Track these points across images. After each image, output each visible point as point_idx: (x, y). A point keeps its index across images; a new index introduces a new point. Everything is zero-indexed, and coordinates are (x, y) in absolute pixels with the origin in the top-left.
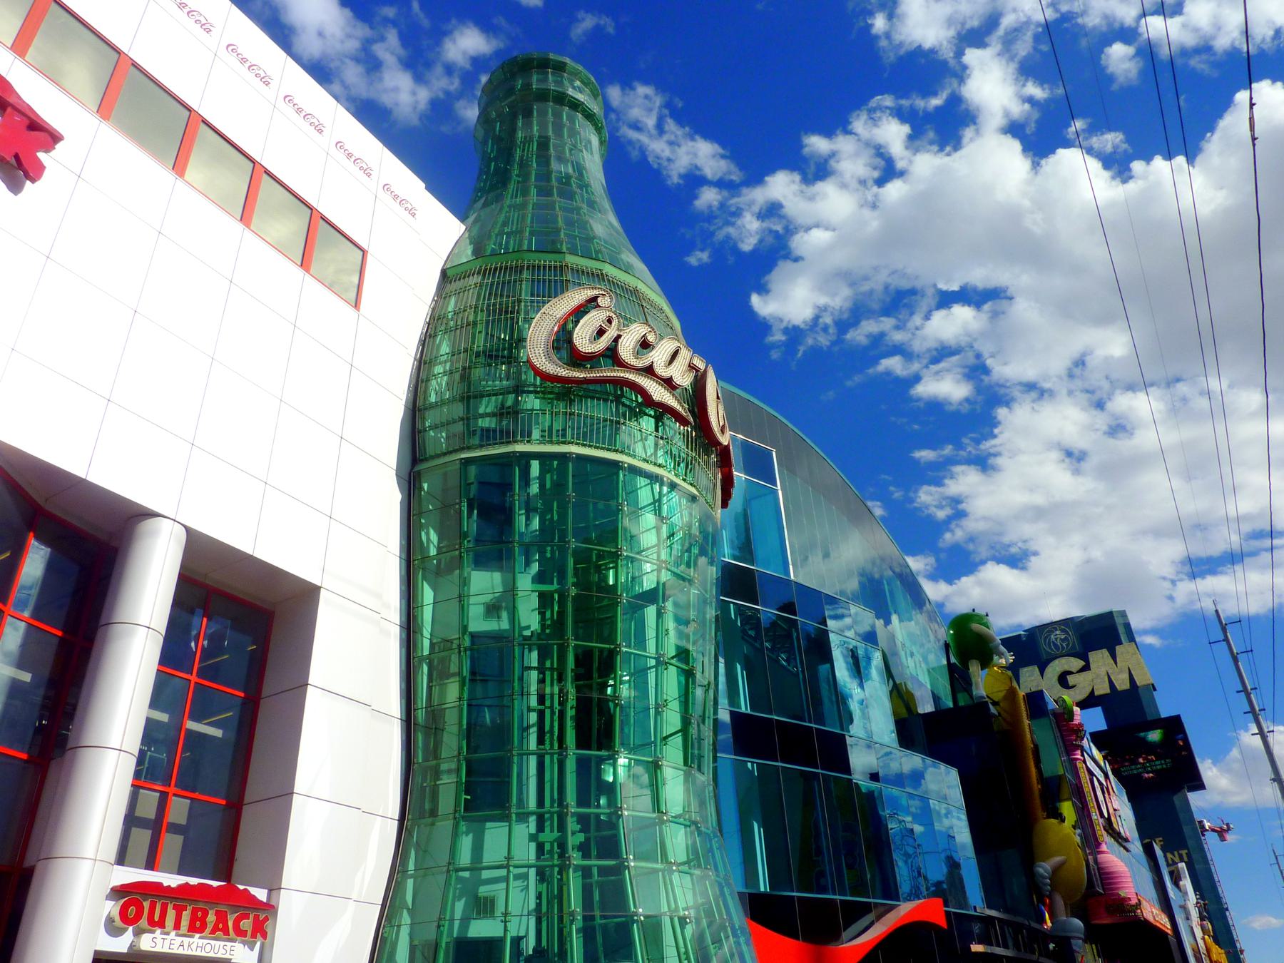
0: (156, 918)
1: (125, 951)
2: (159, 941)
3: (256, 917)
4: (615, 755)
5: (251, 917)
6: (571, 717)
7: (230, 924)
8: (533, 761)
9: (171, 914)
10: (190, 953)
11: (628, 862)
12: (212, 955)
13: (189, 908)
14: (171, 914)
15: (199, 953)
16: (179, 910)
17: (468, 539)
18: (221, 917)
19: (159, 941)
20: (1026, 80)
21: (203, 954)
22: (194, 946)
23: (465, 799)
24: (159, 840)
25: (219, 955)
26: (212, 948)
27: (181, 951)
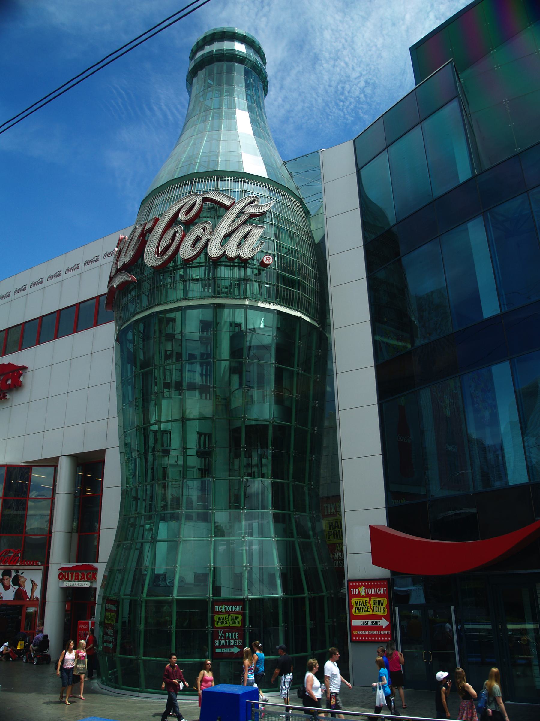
0: (67, 577)
1: (468, 224)
2: (68, 584)
3: (93, 573)
4: (249, 600)
5: (91, 573)
6: (162, 343)
7: (86, 577)
8: (135, 340)
9: (70, 575)
10: (75, 586)
11: (280, 565)
12: (81, 586)
13: (74, 573)
14: (70, 575)
15: (78, 586)
16: (72, 574)
17: (151, 521)
18: (83, 574)
19: (68, 584)
20: (380, 706)
21: (79, 586)
22: (76, 584)
23: (94, 615)
24: (268, 442)
25: (83, 586)
26: (81, 584)
27: (73, 586)
